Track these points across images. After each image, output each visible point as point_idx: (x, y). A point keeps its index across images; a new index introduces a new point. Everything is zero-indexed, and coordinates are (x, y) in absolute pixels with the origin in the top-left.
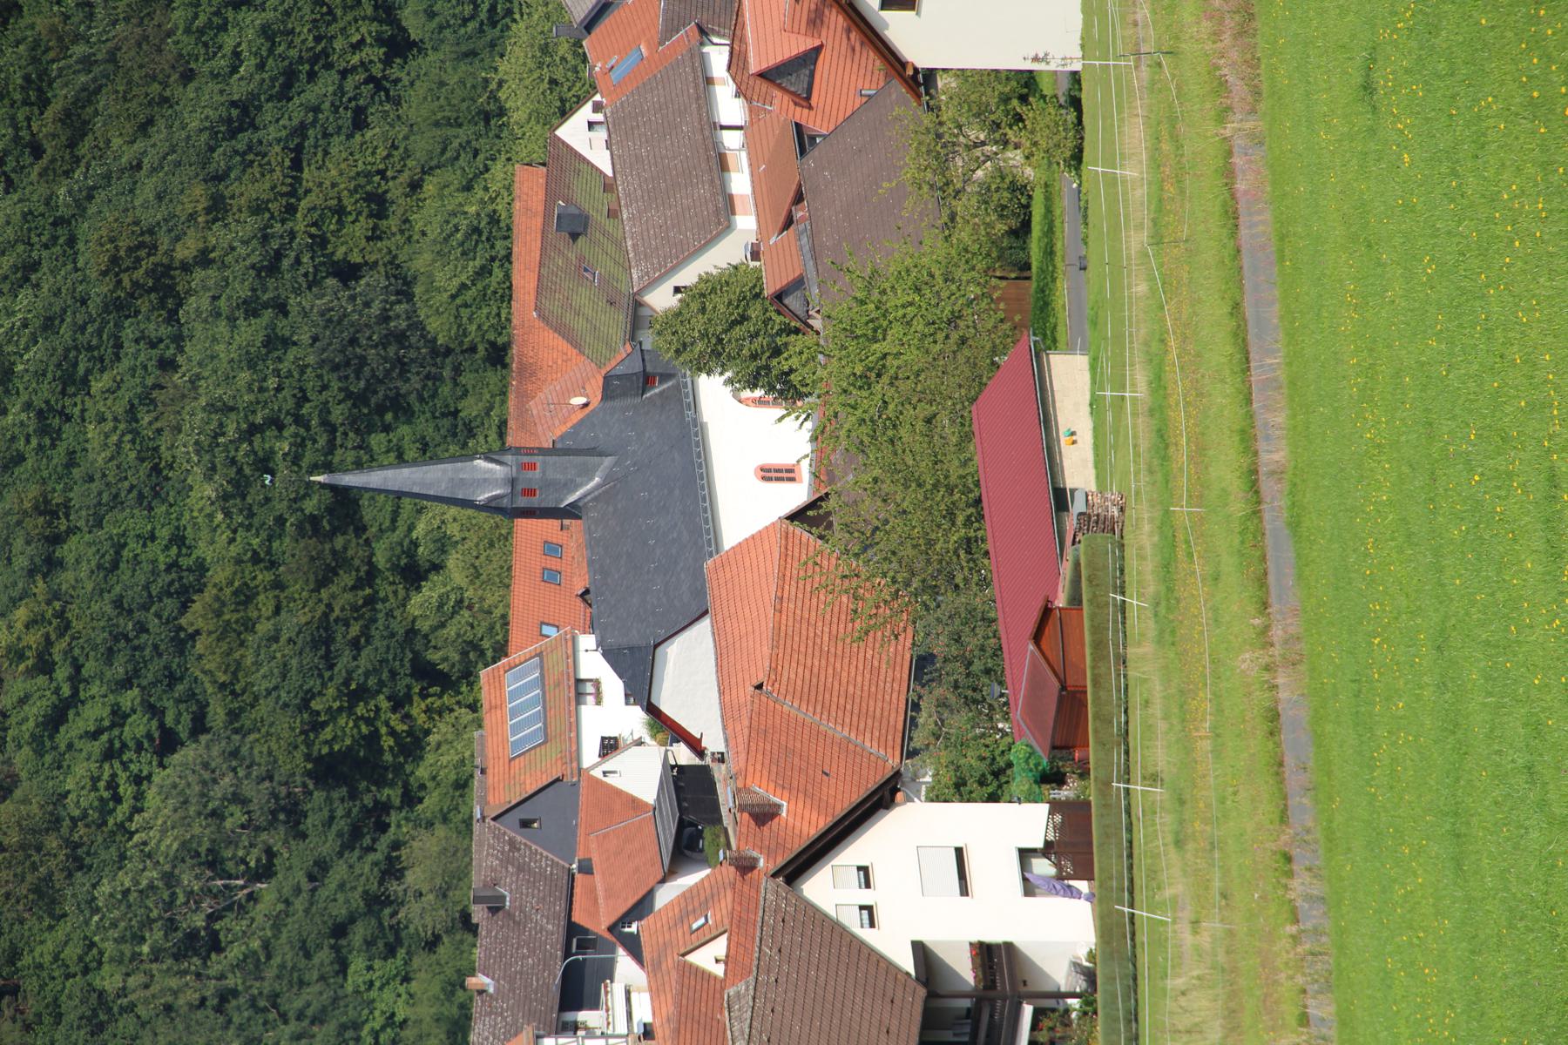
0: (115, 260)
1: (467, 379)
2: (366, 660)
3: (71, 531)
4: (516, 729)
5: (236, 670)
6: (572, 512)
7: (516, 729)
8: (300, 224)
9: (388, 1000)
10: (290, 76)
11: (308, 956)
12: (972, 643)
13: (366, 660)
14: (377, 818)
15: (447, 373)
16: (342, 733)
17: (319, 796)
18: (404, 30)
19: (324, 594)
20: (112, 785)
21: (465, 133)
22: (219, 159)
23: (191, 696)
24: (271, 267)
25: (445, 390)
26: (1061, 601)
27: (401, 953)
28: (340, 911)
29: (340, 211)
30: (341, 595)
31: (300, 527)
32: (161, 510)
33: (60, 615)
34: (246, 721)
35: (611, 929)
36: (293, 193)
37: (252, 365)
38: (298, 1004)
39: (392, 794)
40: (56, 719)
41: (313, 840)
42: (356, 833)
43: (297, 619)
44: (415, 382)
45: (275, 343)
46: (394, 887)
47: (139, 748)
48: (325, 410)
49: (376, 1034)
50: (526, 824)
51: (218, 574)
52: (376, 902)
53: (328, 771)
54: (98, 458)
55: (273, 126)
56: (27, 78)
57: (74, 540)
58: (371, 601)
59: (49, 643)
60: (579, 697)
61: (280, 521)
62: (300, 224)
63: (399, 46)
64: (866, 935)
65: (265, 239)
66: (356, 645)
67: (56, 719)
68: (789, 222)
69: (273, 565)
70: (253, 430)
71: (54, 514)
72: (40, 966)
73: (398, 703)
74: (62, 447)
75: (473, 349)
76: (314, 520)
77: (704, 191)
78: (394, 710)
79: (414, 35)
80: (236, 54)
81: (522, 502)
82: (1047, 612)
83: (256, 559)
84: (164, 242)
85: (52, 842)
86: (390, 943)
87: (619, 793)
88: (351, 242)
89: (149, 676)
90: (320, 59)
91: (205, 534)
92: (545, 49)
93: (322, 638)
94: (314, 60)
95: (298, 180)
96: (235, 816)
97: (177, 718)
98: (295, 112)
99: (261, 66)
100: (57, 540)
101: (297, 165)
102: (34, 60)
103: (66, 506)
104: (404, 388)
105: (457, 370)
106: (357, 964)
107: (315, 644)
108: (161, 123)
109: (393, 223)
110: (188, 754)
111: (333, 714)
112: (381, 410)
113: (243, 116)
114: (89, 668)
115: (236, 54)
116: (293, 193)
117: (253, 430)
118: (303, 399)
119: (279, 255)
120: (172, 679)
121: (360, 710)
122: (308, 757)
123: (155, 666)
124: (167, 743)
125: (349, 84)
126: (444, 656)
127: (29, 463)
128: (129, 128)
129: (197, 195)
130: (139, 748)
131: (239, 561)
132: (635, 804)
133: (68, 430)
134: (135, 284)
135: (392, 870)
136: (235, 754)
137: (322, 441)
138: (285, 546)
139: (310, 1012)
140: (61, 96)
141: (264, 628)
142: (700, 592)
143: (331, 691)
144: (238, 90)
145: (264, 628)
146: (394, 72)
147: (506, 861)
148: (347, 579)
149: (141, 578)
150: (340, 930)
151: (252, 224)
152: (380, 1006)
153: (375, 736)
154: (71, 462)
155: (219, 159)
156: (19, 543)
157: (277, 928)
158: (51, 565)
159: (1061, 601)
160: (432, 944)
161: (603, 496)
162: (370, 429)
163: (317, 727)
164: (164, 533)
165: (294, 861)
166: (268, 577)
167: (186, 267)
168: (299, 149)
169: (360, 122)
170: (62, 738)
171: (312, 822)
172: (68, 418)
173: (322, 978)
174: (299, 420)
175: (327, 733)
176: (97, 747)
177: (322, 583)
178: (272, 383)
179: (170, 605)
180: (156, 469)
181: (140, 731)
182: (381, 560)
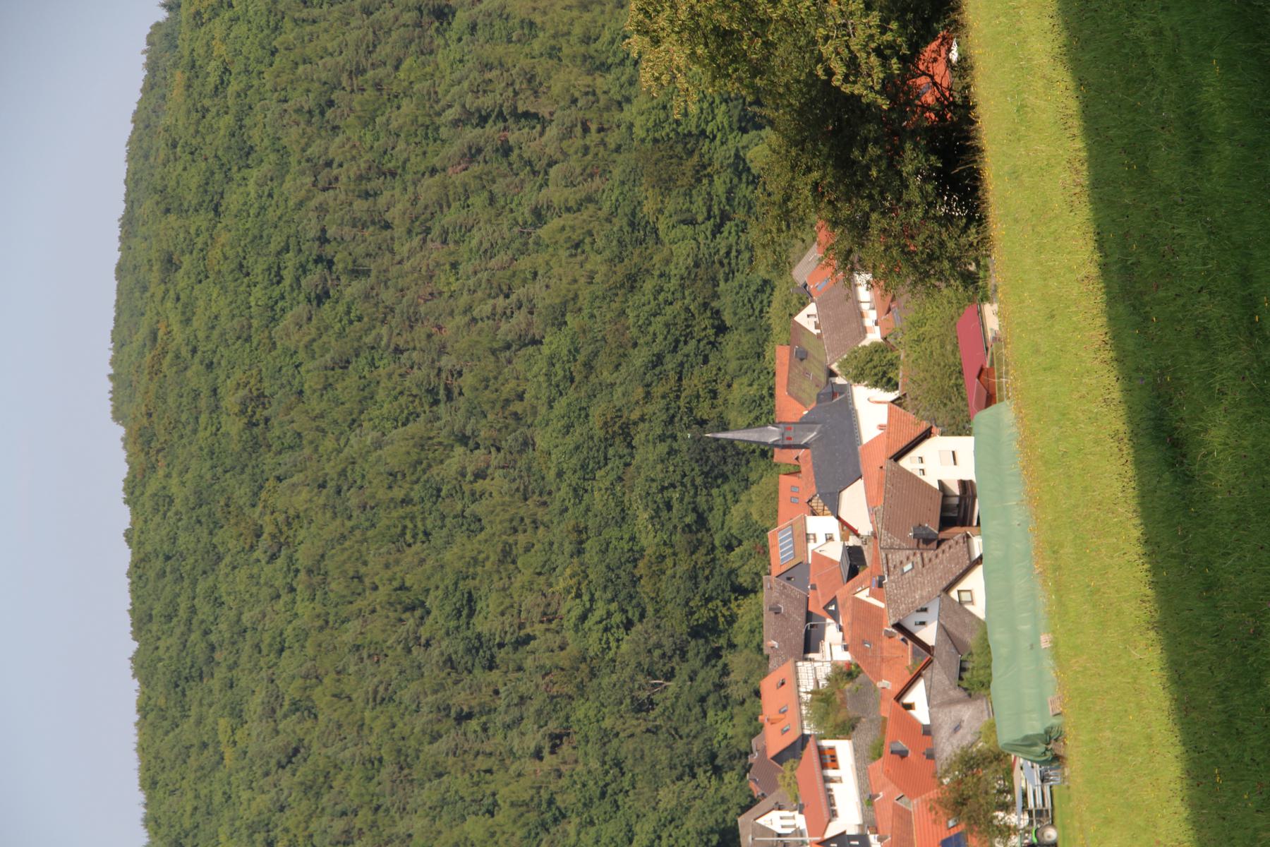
0: (606, 423)
1: (752, 464)
2: (711, 585)
3: (588, 538)
4: (783, 554)
5: (658, 591)
6: (805, 446)
7: (783, 554)
8: (682, 403)
9: (724, 728)
10: (677, 341)
11: (690, 710)
12: (959, 419)
13: (711, 585)
14: (716, 654)
15: (744, 462)
16: (703, 615)
17: (693, 643)
18: (723, 321)
19: (694, 557)
20: (608, 642)
21: (751, 361)
22: (648, 378)
23: (639, 605)
24: (671, 420)
25: (743, 469)
26: (988, 366)
27: (729, 708)
28: (703, 691)
29: (698, 396)
30: (700, 557)
31: (683, 531)
32: (625, 527)
33: (584, 572)
34: (662, 614)
35: (825, 608)
36: (679, 390)
37: (662, 461)
38: (687, 730)
39: (722, 642)
40: (583, 617)
41: (691, 662)
42: (708, 659)
43: (682, 568)
44: (730, 467)
45: (672, 452)
46: (726, 680)
47: (618, 627)
48: (693, 481)
49: (719, 743)
50: (789, 579)
51: (649, 551)
52: (720, 686)
53: (696, 633)
54: (598, 506)
55: (670, 363)
56: (570, 351)
57: (589, 542)
58: (713, 560)
59: (579, 584)
60: (808, 540)
61: (675, 527)
62: (682, 403)
63: (721, 329)
64: (922, 477)
65: (667, 409)
66: (707, 579)
67: (583, 617)
68: (889, 310)
69: (672, 546)
70: (663, 489)
71: (580, 532)
72: (579, 721)
73: (725, 603)
74: (584, 503)
75: (754, 451)
76: (688, 526)
77: (854, 325)
78: (724, 605)
79: (728, 324)
80: (655, 334)
81: (787, 442)
82: (982, 370)
83: (665, 544)
84: (626, 414)
85: (583, 666)
86: (725, 703)
87: (825, 558)
88: (703, 410)
89: (622, 596)
90: (688, 336)
91: (644, 535)
92: (787, 302)
93: (693, 576)
94: (686, 336)
95: (680, 386)
96: (657, 653)
97: (633, 614)
98: (679, 357)
99: (665, 339)
100: (581, 542)
101: (680, 379)
102: (573, 343)
103: (586, 528)
104: (725, 469)
105: (748, 462)
106: (711, 713)
107: (691, 578)
108: (624, 364)
109: (720, 401)
110: (638, 627)
111: (699, 607)
112: (716, 478)
113: (658, 360)
114: (597, 595)
115: (655, 334)
116: (679, 390)
117: (663, 489)
118: (685, 475)
119: (673, 416)
120: (631, 597)
121: (710, 606)
122: (688, 626)
123: (624, 592)
124: (628, 625)
125: (702, 344)
126: (744, 580)
127: (570, 511)
128: (611, 367)
129: (639, 392)
130: (618, 627)
131: (658, 545)
132: (832, 562)
133: (586, 496)
134: (614, 432)
135: (725, 672)
136: (658, 627)
137: (692, 492)
138: (677, 538)
139: (692, 734)
140: (581, 358)
141: (669, 572)
142: (856, 465)
143: (697, 598)
144: (656, 349)
145: (669, 572)
146: (719, 339)
147: (782, 593)
148: (703, 550)
149: (617, 555)
150: (703, 700)
151: (663, 403)
152: (722, 731)
153: (716, 617)
154: (588, 510)
155: (648, 378)
156: (566, 544)
157: (677, 698)
158: (580, 552)
159: (988, 366)
160: (743, 703)
161: (818, 440)
162: (712, 487)
163: (692, 613)
164: (626, 537)
165: (683, 671)
166: (671, 551)
167: (635, 423)
168: (680, 373)
169: (706, 360)
170: (587, 624)
171: (690, 655)
172: (586, 491)
173: (697, 720)
174: (683, 484)
175: (696, 616)
176: (601, 626)
177: (692, 553)
178: (671, 469)
179: (629, 566)
180: (623, 510)
181: (618, 620)
182: (717, 543)
